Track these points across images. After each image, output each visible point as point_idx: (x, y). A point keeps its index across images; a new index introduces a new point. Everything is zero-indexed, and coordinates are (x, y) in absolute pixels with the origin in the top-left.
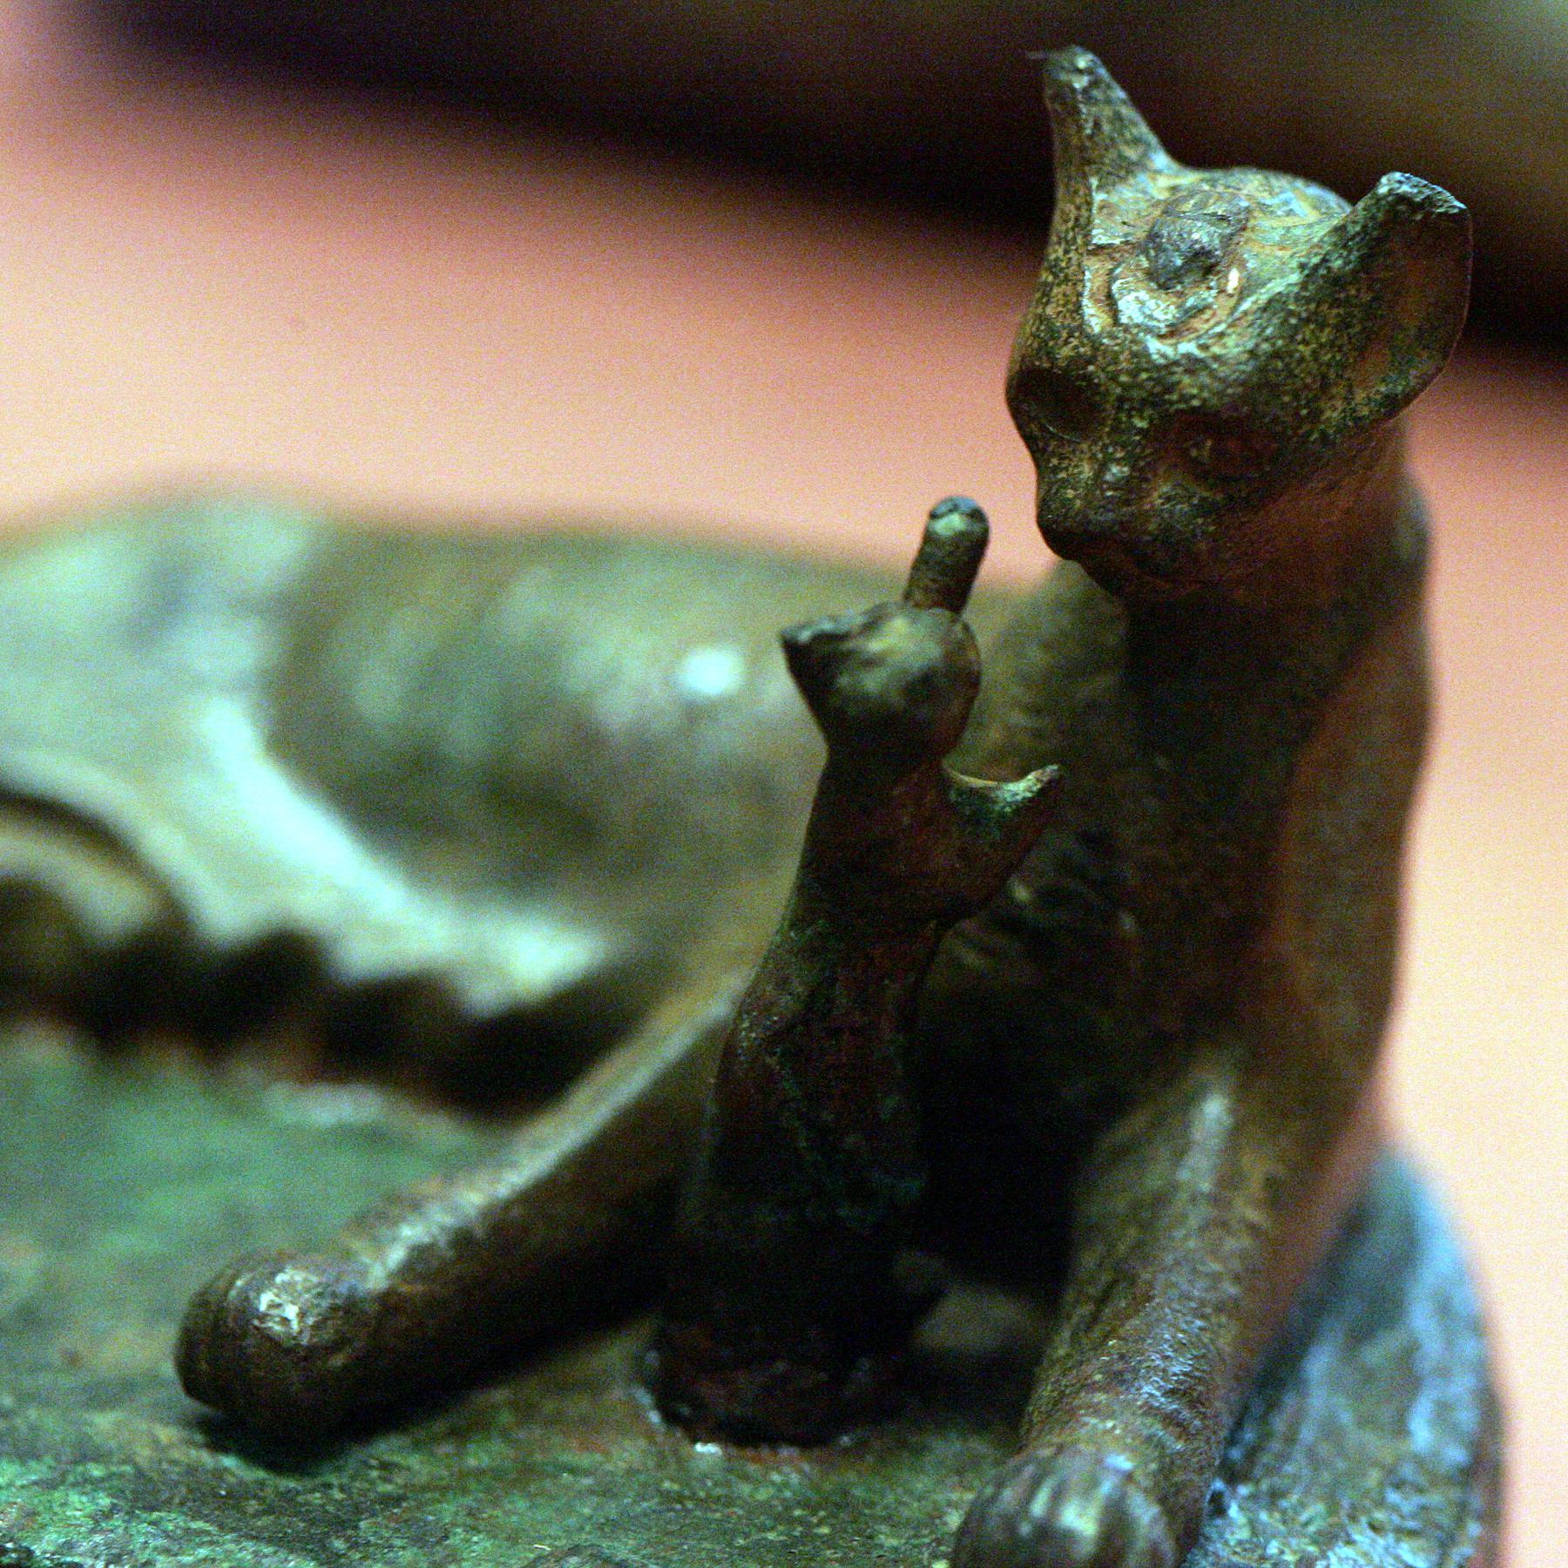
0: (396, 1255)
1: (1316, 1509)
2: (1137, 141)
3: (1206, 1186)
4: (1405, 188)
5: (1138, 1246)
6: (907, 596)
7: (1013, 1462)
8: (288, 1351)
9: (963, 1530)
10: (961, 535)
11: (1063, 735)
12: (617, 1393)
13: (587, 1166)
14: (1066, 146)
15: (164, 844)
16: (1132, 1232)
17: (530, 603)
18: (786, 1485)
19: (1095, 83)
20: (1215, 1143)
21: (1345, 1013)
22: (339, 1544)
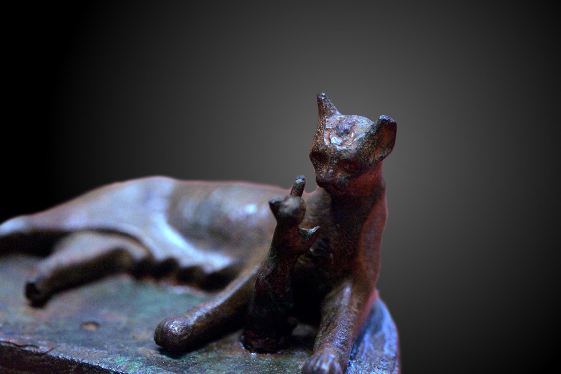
0: (195, 318)
1: (368, 365)
2: (334, 109)
3: (346, 304)
4: (385, 118)
5: (334, 315)
7: (312, 356)
8: (176, 336)
9: (304, 369)
10: (301, 183)
11: (320, 220)
12: (236, 344)
13: (231, 301)
15: (149, 241)
16: (333, 313)
18: (269, 361)
19: (326, 98)
20: (348, 297)
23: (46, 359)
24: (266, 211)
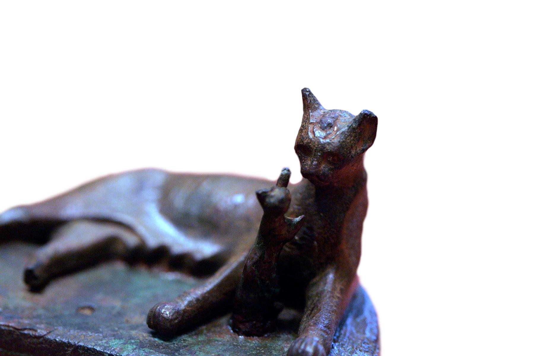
0: (186, 303)
1: (350, 347)
3: (330, 290)
5: (318, 300)
6: (277, 185)
7: (297, 339)
8: (167, 320)
9: (289, 351)
11: (304, 210)
12: (224, 327)
13: (219, 286)
15: (141, 229)
16: (317, 298)
17: (206, 187)
18: (256, 343)
20: (332, 282)
21: (354, 259)
23: (44, 342)
24: (253, 201)
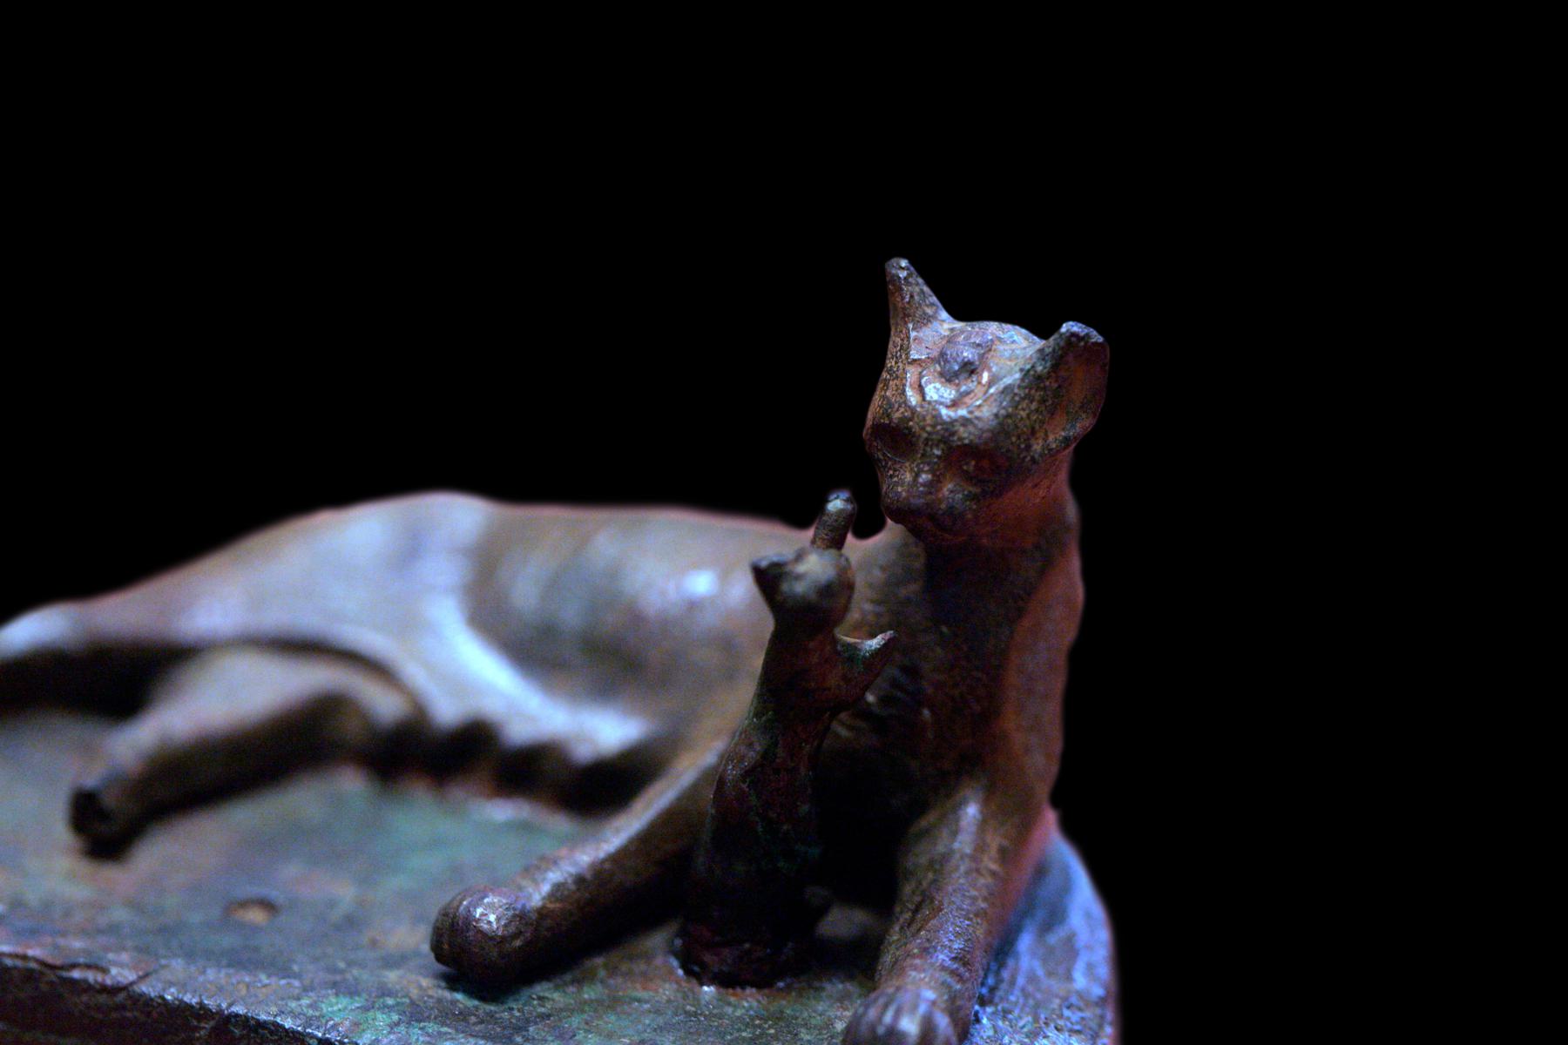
0: (546, 888)
1: (1027, 1019)
2: (932, 304)
3: (968, 850)
5: (935, 881)
7: (873, 995)
8: (492, 939)
9: (848, 1030)
11: (893, 615)
12: (659, 961)
13: (644, 840)
14: (896, 309)
15: (415, 674)
16: (930, 875)
18: (751, 1007)
19: (910, 275)
20: (973, 829)
22: (519, 1039)
23: (129, 1003)
